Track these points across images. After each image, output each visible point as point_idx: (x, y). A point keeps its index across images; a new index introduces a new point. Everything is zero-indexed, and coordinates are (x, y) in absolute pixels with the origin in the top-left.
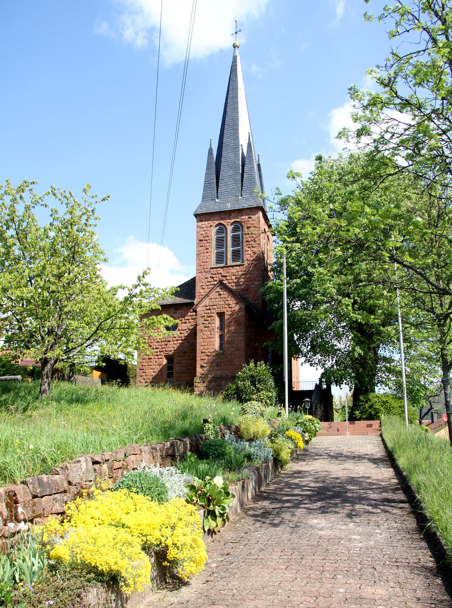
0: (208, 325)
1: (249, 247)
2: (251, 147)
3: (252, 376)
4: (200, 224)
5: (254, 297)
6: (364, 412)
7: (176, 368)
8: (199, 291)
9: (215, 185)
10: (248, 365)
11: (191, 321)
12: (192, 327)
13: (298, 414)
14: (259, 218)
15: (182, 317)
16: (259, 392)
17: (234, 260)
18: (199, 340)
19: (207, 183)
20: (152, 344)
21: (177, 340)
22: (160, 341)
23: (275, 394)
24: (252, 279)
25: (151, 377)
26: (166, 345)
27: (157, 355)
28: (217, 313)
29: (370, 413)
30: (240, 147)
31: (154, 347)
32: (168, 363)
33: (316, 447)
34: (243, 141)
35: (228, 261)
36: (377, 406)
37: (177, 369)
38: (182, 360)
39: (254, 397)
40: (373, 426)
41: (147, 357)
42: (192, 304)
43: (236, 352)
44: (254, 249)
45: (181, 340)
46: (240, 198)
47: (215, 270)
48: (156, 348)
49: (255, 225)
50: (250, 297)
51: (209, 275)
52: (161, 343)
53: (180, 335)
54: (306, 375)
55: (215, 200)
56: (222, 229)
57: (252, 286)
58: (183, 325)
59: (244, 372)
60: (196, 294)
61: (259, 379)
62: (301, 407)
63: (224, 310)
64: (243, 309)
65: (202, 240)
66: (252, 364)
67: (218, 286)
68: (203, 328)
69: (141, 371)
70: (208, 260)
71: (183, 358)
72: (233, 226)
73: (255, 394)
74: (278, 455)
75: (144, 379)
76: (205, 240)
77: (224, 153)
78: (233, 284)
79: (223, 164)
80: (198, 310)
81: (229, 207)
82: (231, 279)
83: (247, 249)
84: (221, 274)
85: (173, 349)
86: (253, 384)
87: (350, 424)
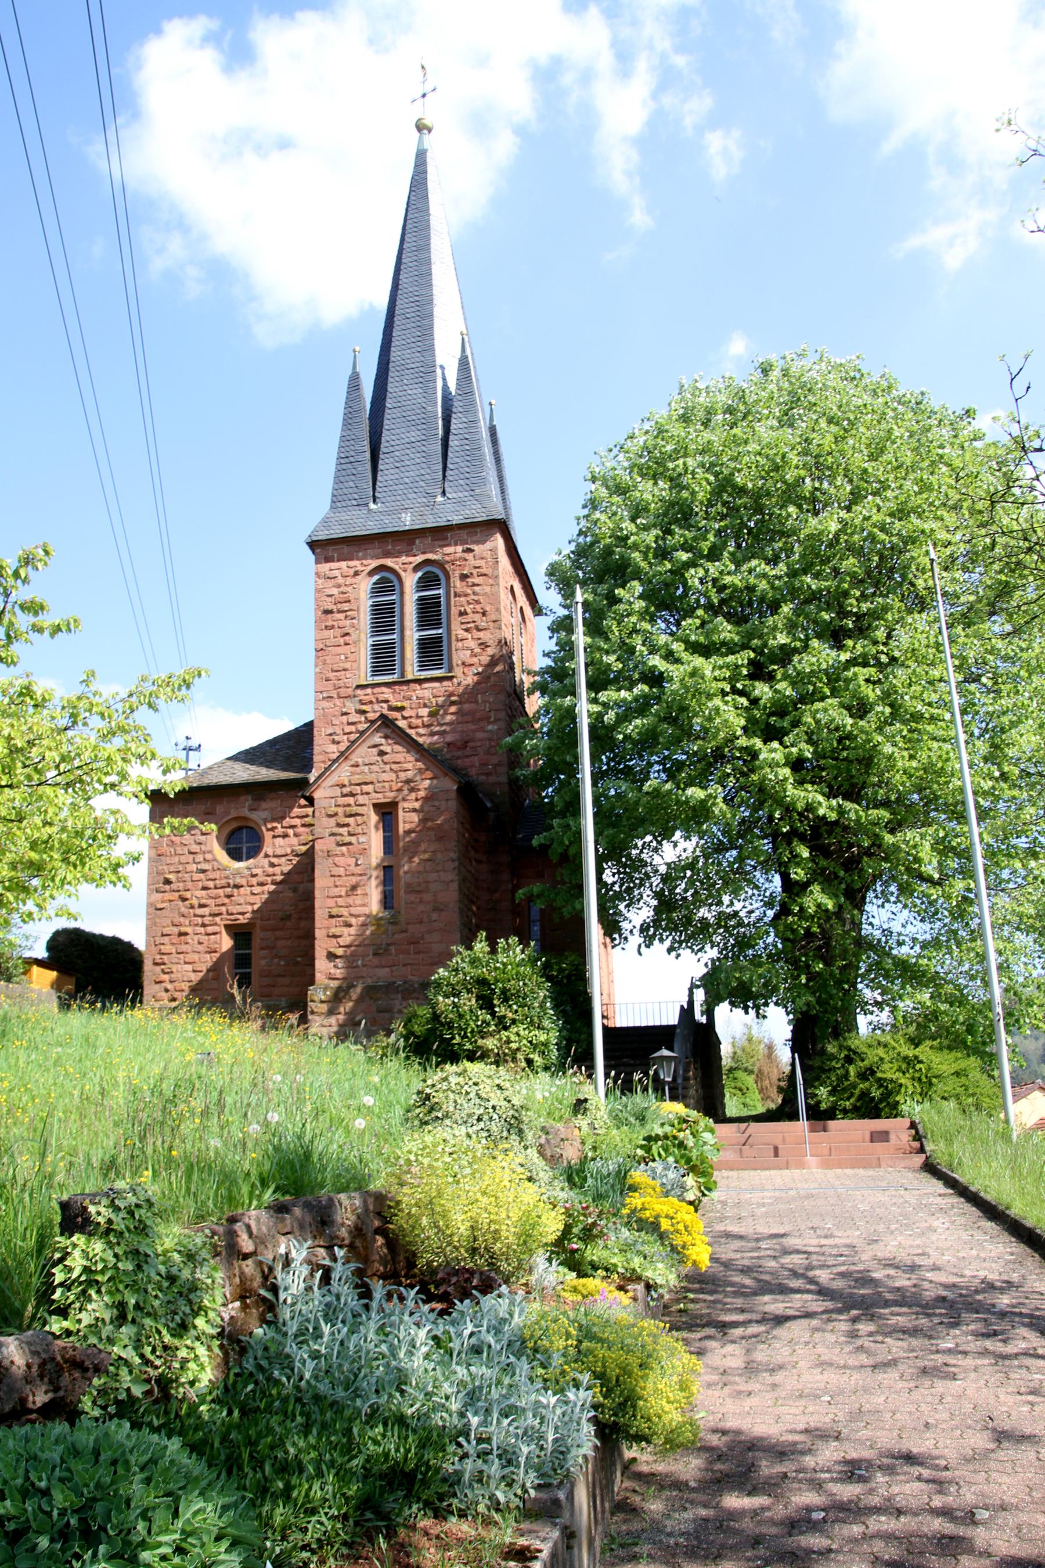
0: (347, 839)
1: (467, 630)
2: (468, 369)
3: (482, 982)
4: (325, 567)
5: (484, 764)
6: (844, 1090)
7: (260, 961)
8: (323, 748)
9: (368, 466)
10: (470, 948)
11: (301, 830)
12: (304, 848)
13: (638, 1100)
14: (494, 551)
15: (274, 820)
16: (506, 1028)
17: (423, 666)
18: (321, 881)
19: (344, 461)
20: (188, 895)
21: (262, 884)
22: (211, 884)
23: (553, 1037)
24: (478, 715)
25: (186, 986)
26: (229, 896)
27: (204, 925)
28: (375, 805)
29: (864, 1094)
30: (439, 371)
31: (195, 902)
32: (236, 946)
33: (734, 1228)
34: (446, 355)
35: (408, 668)
36: (889, 1072)
37: (263, 962)
38: (277, 939)
39: (490, 1043)
40: (892, 1136)
41: (176, 930)
42: (304, 783)
43: (434, 916)
44: (481, 634)
45: (273, 883)
46: (440, 499)
47: (369, 691)
48: (201, 906)
49: (484, 571)
50: (472, 765)
51: (351, 706)
52: (213, 892)
53: (271, 870)
54: (641, 981)
55: (366, 505)
56: (387, 582)
57: (480, 735)
58: (279, 841)
59: (456, 970)
60: (316, 758)
61: (504, 991)
62: (646, 1074)
64: (453, 795)
65: (330, 612)
66: (480, 946)
67: (377, 730)
68: (332, 846)
69: (158, 969)
70: (348, 665)
71: (278, 933)
72: (420, 574)
73: (491, 1034)
74: (629, 1402)
75: (167, 990)
76: (339, 612)
77: (391, 388)
78: (422, 731)
79: (388, 414)
80: (316, 795)
81: (407, 521)
82: (418, 717)
83: (462, 634)
84: (386, 701)
85: (249, 908)
86: (486, 1003)
87: (812, 1130)
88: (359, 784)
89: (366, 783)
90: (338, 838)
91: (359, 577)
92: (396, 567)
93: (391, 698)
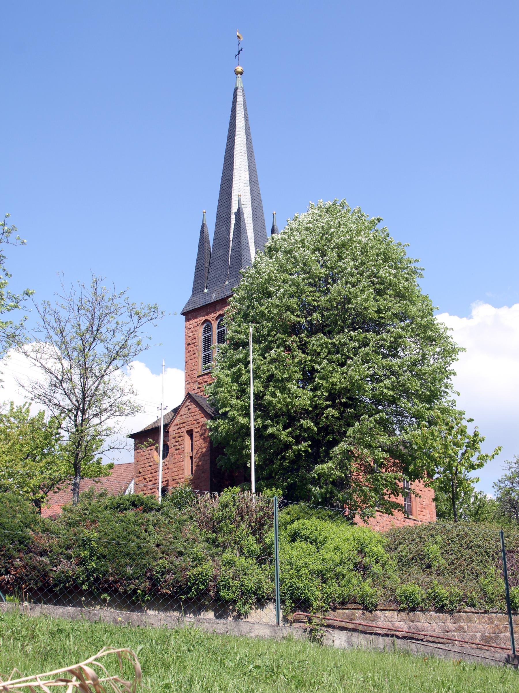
20: (146, 477)
28: (187, 431)
47: (201, 378)
48: (150, 481)
63: (192, 427)
70: (194, 368)
84: (206, 382)
88: (182, 424)
89: (184, 423)
90: (176, 447)
91: (198, 327)
92: (210, 320)
93: (208, 380)
